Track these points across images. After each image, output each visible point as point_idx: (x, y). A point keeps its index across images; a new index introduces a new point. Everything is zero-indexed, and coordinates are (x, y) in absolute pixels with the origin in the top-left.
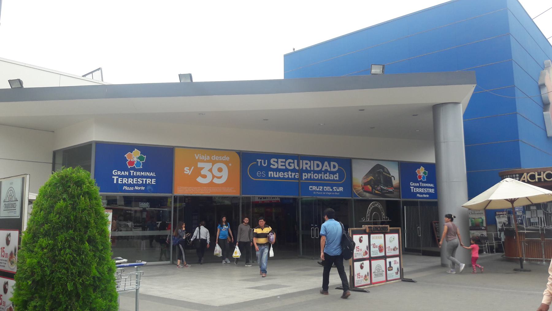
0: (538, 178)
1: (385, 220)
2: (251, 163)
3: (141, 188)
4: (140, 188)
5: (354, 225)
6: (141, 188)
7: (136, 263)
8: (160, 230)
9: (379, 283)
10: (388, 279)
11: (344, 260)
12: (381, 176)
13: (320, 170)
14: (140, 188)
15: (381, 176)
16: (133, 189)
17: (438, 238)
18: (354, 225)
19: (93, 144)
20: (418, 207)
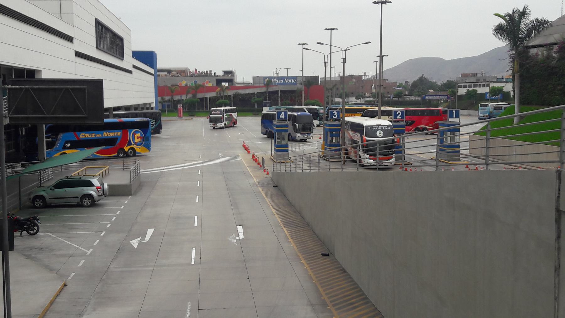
0: (46, 141)
1: (45, 140)
2: (137, 129)
3: (291, 81)
4: (290, 81)
5: (286, 128)
6: (291, 81)
7: (516, 106)
8: (486, 93)
9: (350, 295)
10: (376, 62)
11: (478, 93)
12: (51, 136)
13: (382, 130)
14: (290, 81)
15: (51, 136)
16: (282, 82)
17: (409, 118)
18: (286, 128)
19: (77, 50)
20: (327, 126)
